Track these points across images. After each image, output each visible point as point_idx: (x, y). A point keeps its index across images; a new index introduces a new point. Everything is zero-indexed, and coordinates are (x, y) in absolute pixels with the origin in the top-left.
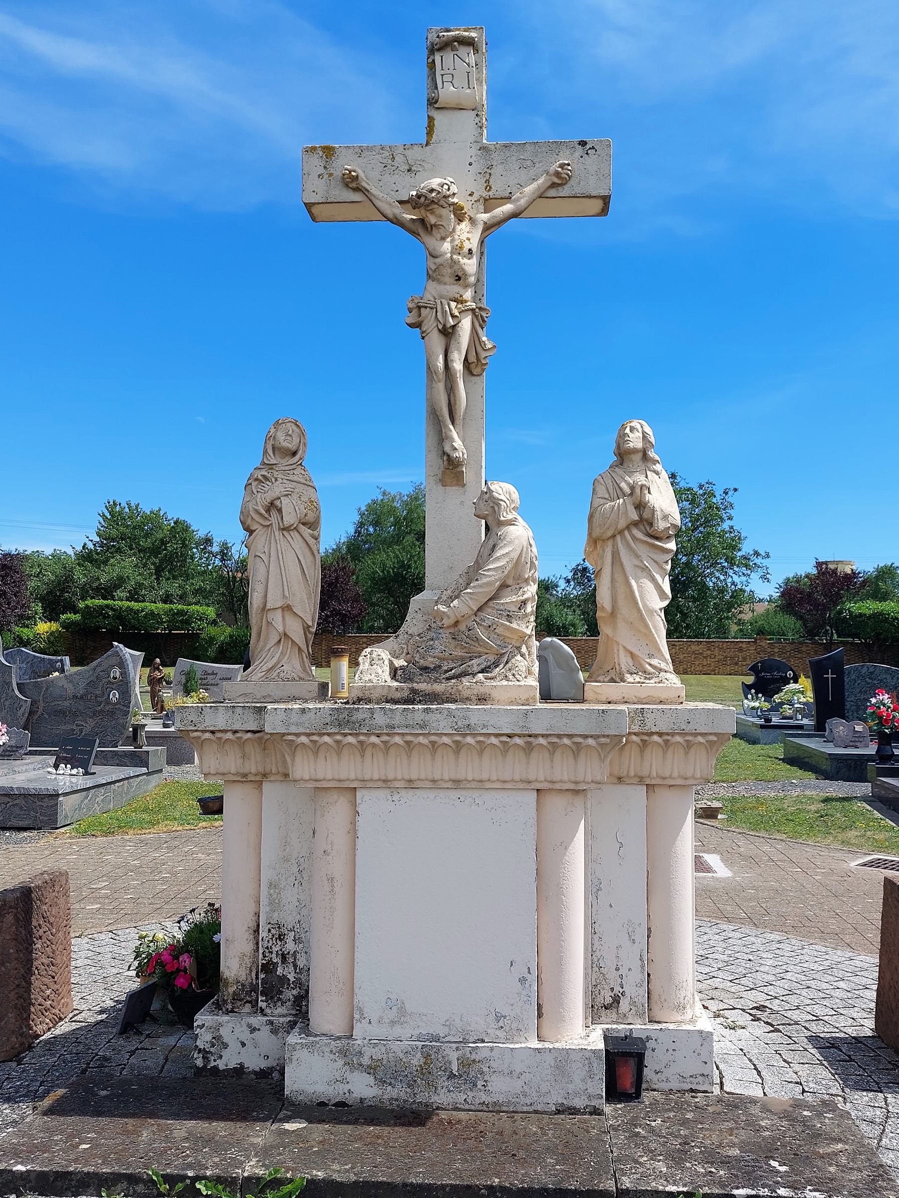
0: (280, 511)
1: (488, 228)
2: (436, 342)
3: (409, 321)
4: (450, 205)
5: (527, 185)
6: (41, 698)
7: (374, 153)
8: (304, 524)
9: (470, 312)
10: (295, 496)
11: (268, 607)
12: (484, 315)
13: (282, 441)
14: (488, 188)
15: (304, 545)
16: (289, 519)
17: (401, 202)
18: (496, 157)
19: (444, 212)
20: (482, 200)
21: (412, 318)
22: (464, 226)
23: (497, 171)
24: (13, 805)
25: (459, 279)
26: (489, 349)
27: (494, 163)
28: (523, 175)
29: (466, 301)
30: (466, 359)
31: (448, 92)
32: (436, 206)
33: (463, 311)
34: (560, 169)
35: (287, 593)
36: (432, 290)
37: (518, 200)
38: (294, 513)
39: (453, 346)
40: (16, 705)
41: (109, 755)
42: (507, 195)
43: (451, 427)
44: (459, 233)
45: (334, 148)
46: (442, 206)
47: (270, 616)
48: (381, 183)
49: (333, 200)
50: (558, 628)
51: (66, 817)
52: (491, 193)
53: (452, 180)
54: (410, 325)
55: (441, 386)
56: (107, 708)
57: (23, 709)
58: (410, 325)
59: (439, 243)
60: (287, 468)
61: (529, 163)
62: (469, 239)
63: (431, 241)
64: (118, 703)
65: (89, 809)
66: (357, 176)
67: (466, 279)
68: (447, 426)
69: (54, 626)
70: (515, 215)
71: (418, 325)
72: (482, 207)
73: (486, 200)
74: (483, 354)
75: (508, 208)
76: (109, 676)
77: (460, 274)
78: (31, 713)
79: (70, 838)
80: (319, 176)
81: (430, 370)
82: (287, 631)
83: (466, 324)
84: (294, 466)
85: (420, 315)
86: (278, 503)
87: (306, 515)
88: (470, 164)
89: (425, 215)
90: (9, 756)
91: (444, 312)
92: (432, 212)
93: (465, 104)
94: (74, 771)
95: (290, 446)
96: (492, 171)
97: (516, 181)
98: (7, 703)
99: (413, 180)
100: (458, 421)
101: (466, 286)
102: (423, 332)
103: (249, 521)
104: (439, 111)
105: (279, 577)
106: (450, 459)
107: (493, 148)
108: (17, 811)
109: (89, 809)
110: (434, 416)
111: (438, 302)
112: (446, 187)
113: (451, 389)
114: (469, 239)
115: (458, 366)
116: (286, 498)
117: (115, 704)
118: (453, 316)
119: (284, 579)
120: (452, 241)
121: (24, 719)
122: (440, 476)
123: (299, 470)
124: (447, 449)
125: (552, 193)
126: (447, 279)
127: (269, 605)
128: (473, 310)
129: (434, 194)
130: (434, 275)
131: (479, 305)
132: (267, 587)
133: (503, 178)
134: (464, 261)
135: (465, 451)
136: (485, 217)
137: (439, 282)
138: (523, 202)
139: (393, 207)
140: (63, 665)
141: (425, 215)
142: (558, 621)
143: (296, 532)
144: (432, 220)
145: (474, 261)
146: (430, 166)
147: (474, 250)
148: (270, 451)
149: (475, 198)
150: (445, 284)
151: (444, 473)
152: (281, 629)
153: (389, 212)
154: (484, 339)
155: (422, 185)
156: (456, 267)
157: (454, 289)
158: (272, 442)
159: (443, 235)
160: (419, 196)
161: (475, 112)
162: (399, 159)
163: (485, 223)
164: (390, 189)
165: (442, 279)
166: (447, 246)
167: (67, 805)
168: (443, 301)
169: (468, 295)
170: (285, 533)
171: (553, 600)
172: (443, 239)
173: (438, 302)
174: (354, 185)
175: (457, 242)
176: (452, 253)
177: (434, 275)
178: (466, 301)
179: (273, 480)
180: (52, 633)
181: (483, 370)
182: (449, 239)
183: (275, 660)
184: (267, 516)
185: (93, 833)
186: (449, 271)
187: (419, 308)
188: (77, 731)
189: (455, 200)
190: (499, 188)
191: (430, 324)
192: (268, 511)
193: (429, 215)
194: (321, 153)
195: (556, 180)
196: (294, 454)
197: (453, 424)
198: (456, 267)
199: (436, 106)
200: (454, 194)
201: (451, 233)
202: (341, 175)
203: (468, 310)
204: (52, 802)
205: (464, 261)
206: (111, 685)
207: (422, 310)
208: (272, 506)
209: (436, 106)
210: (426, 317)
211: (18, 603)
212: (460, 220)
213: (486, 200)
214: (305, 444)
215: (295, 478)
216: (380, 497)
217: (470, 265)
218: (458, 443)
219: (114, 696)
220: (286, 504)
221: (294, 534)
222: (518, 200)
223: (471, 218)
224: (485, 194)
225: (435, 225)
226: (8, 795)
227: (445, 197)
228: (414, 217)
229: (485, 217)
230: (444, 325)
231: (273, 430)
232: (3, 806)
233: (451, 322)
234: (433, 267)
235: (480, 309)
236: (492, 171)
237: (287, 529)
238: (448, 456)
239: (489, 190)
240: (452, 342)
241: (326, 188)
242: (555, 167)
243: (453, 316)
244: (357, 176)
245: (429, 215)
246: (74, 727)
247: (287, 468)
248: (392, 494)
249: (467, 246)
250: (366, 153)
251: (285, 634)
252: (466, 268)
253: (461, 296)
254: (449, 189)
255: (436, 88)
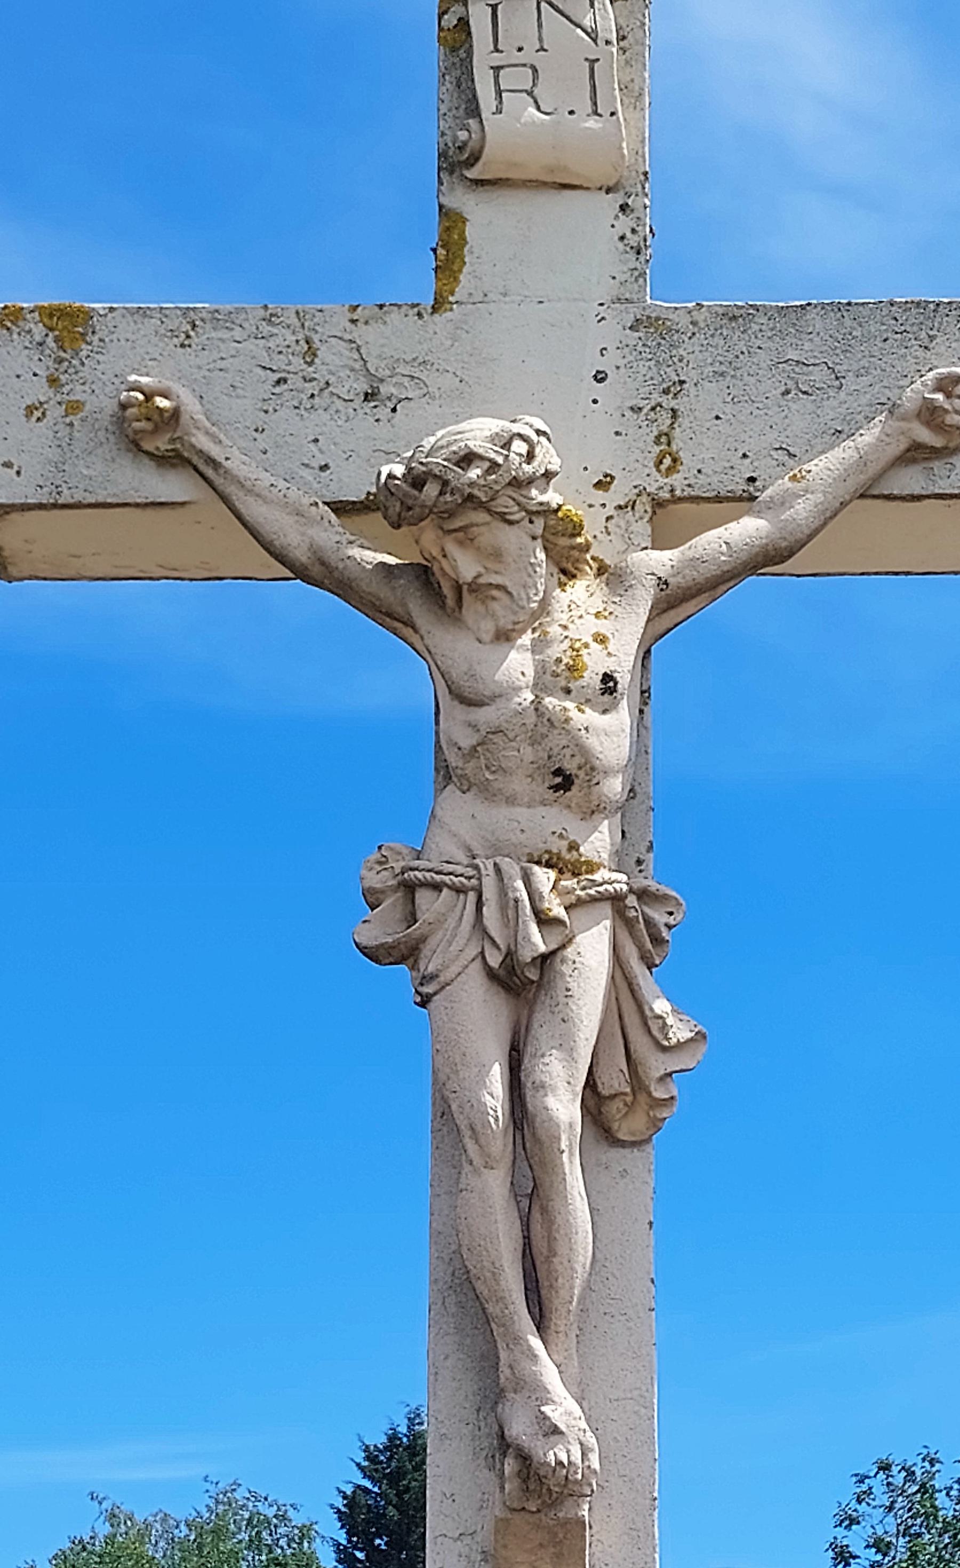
1: (673, 600)
2: (477, 1015)
3: (371, 935)
4: (532, 515)
5: (813, 453)
7: (238, 333)
9: (607, 908)
12: (659, 917)
14: (667, 461)
17: (340, 508)
18: (695, 356)
19: (511, 539)
20: (643, 505)
21: (379, 928)
22: (583, 593)
23: (700, 401)
25: (564, 782)
26: (680, 1045)
27: (690, 375)
28: (799, 418)
29: (592, 867)
30: (590, 1084)
31: (515, 125)
32: (481, 517)
33: (580, 902)
34: (940, 397)
36: (461, 825)
37: (784, 501)
39: (542, 1031)
42: (740, 487)
43: (535, 1342)
44: (564, 618)
45: (88, 315)
46: (504, 518)
48: (263, 441)
49: (79, 496)
52: (677, 480)
53: (543, 427)
54: (372, 954)
55: (493, 1187)
58: (372, 954)
59: (488, 652)
61: (819, 375)
62: (601, 639)
63: (457, 647)
66: (176, 414)
67: (592, 783)
68: (518, 1340)
70: (766, 559)
71: (405, 953)
72: (642, 529)
73: (658, 504)
74: (656, 1065)
75: (747, 530)
77: (570, 766)
80: (30, 410)
81: (449, 1121)
83: (592, 949)
85: (412, 919)
88: (600, 377)
89: (435, 547)
91: (509, 906)
92: (465, 537)
93: (580, 170)
96: (680, 404)
97: (772, 438)
99: (383, 430)
100: (564, 1315)
101: (593, 811)
102: (426, 979)
104: (483, 194)
106: (529, 1470)
107: (684, 321)
110: (464, 1299)
111: (487, 868)
112: (519, 447)
113: (534, 1196)
114: (601, 639)
115: (563, 1107)
118: (544, 920)
120: (538, 646)
122: (486, 1537)
124: (519, 1428)
125: (911, 480)
126: (519, 784)
128: (616, 899)
129: (474, 473)
130: (470, 768)
131: (640, 882)
133: (721, 425)
134: (584, 718)
135: (591, 1440)
136: (662, 560)
137: (488, 793)
138: (802, 510)
139: (311, 522)
141: (435, 547)
144: (466, 566)
145: (622, 717)
146: (448, 381)
147: (624, 680)
149: (619, 493)
150: (511, 801)
151: (502, 1526)
153: (295, 538)
154: (661, 1006)
155: (429, 442)
156: (556, 740)
157: (547, 822)
159: (505, 622)
160: (416, 480)
161: (617, 199)
162: (332, 356)
163: (663, 583)
164: (303, 460)
165: (498, 782)
166: (518, 664)
168: (506, 863)
169: (599, 842)
172: (505, 637)
173: (487, 868)
174: (161, 444)
175: (556, 651)
176: (539, 687)
177: (470, 768)
178: (592, 867)
181: (656, 1124)
182: (526, 639)
186: (528, 753)
187: (409, 888)
189: (552, 497)
190: (706, 459)
191: (453, 950)
193: (452, 548)
194: (39, 331)
195: (925, 435)
197: (541, 1327)
198: (556, 740)
199: (471, 174)
200: (548, 475)
201: (535, 615)
202: (111, 406)
203: (594, 900)
205: (584, 718)
207: (423, 897)
209: (471, 174)
210: (440, 920)
212: (567, 573)
213: (658, 504)
216: (104, 1529)
217: (608, 734)
218: (563, 1408)
222: (784, 501)
223: (602, 570)
224: (656, 483)
225: (475, 587)
227: (517, 483)
228: (392, 560)
229: (662, 560)
230: (510, 955)
233: (537, 941)
234: (466, 740)
235: (643, 895)
236: (680, 404)
238: (525, 1458)
239: (670, 471)
240: (538, 1017)
241: (53, 454)
242: (919, 389)
243: (544, 920)
244: (176, 414)
245: (452, 548)
248: (139, 1518)
249: (596, 663)
250: (206, 333)
252: (592, 742)
253: (574, 847)
254: (530, 457)
255: (474, 111)
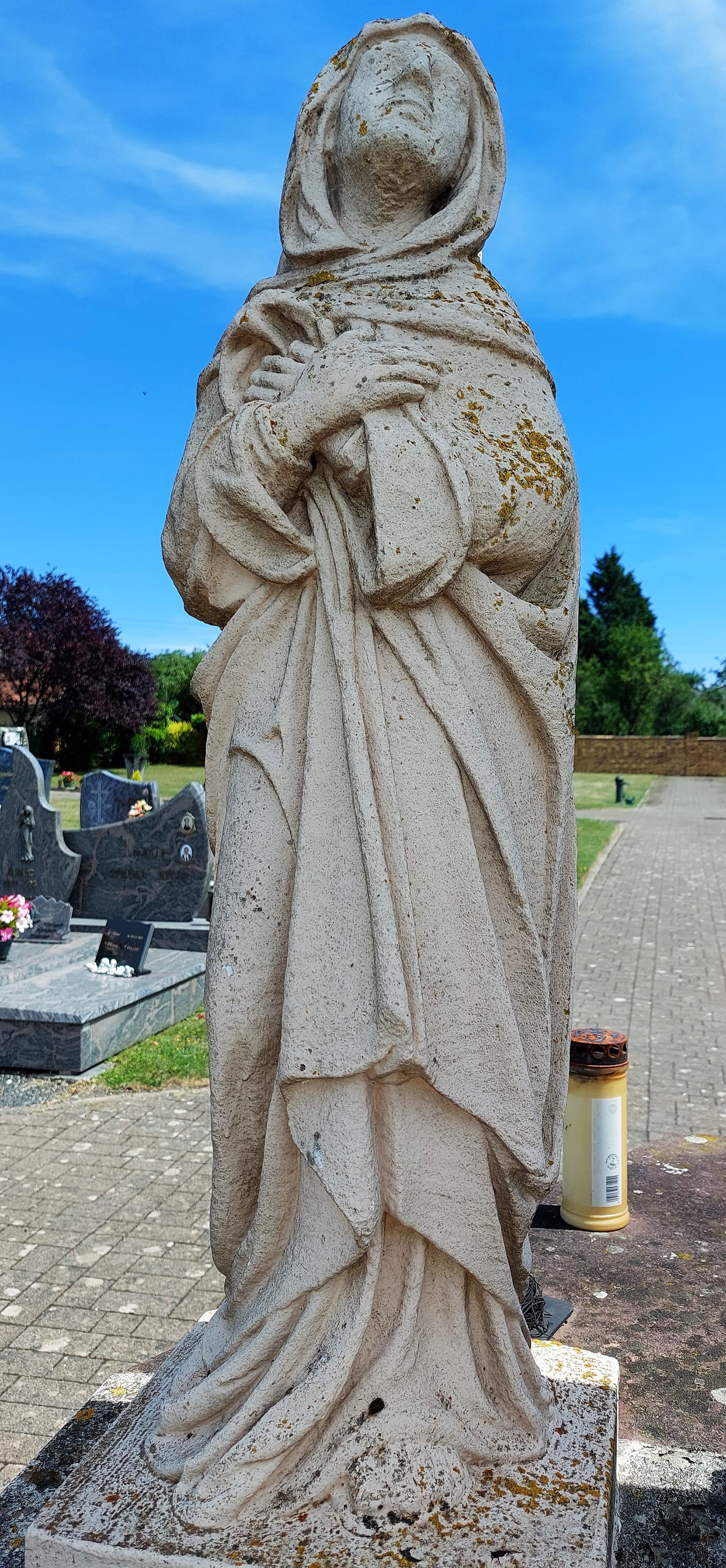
0: (359, 493)
6: (94, 852)
8: (494, 568)
10: (443, 410)
11: (288, 1069)
13: (372, 115)
15: (493, 688)
16: (414, 534)
24: (20, 1036)
35: (396, 997)
38: (436, 503)
40: (61, 863)
41: (178, 936)
47: (306, 1114)
50: (706, 725)
51: (96, 1053)
56: (177, 868)
57: (69, 869)
60: (400, 268)
64: (192, 861)
65: (134, 1032)
69: (185, 726)
76: (180, 825)
78: (82, 872)
79: (96, 1093)
82: (400, 1209)
84: (440, 257)
86: (345, 447)
87: (507, 514)
90: (45, 937)
94: (121, 970)
95: (417, 135)
98: (50, 861)
103: (199, 563)
105: (350, 883)
108: (25, 1044)
109: (134, 1032)
116: (393, 419)
117: (187, 864)
119: (384, 906)
121: (72, 882)
123: (461, 280)
127: (295, 1057)
132: (284, 928)
140: (150, 792)
142: (705, 717)
143: (447, 620)
148: (315, 191)
152: (363, 1209)
158: (323, 140)
167: (95, 1037)
170: (388, 621)
171: (698, 694)
179: (326, 326)
180: (184, 734)
183: (330, 1381)
184: (286, 524)
185: (130, 1085)
188: (139, 898)
192: (296, 499)
196: (439, 196)
204: (72, 1035)
206: (180, 838)
208: (318, 472)
211: (147, 704)
214: (493, 152)
215: (445, 315)
219: (186, 851)
220: (391, 453)
221: (440, 626)
226: (12, 1023)
231: (329, 77)
232: (7, 1037)
237: (392, 600)
246: (136, 893)
247: (400, 268)
251: (388, 1220)
